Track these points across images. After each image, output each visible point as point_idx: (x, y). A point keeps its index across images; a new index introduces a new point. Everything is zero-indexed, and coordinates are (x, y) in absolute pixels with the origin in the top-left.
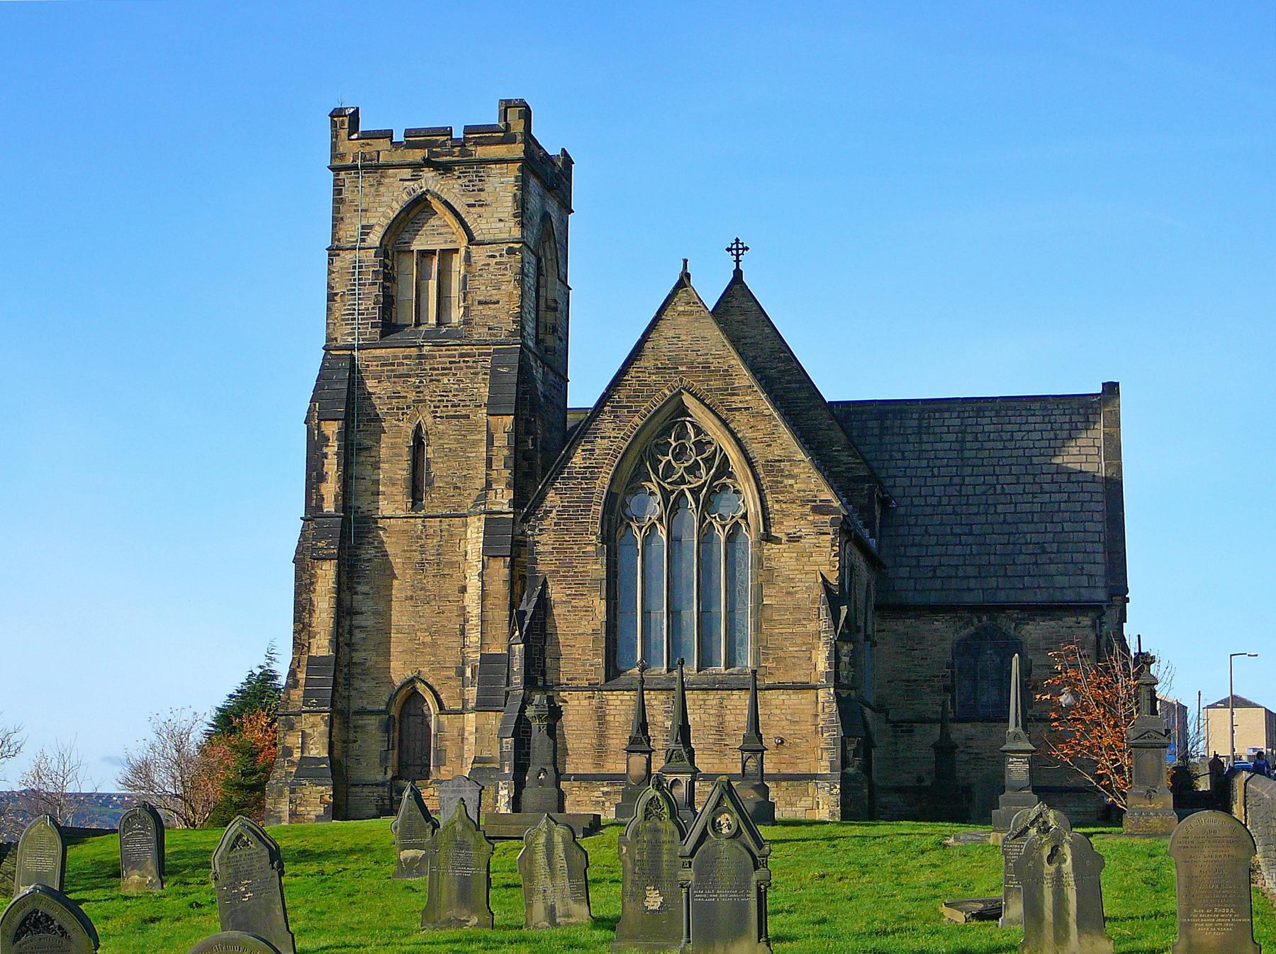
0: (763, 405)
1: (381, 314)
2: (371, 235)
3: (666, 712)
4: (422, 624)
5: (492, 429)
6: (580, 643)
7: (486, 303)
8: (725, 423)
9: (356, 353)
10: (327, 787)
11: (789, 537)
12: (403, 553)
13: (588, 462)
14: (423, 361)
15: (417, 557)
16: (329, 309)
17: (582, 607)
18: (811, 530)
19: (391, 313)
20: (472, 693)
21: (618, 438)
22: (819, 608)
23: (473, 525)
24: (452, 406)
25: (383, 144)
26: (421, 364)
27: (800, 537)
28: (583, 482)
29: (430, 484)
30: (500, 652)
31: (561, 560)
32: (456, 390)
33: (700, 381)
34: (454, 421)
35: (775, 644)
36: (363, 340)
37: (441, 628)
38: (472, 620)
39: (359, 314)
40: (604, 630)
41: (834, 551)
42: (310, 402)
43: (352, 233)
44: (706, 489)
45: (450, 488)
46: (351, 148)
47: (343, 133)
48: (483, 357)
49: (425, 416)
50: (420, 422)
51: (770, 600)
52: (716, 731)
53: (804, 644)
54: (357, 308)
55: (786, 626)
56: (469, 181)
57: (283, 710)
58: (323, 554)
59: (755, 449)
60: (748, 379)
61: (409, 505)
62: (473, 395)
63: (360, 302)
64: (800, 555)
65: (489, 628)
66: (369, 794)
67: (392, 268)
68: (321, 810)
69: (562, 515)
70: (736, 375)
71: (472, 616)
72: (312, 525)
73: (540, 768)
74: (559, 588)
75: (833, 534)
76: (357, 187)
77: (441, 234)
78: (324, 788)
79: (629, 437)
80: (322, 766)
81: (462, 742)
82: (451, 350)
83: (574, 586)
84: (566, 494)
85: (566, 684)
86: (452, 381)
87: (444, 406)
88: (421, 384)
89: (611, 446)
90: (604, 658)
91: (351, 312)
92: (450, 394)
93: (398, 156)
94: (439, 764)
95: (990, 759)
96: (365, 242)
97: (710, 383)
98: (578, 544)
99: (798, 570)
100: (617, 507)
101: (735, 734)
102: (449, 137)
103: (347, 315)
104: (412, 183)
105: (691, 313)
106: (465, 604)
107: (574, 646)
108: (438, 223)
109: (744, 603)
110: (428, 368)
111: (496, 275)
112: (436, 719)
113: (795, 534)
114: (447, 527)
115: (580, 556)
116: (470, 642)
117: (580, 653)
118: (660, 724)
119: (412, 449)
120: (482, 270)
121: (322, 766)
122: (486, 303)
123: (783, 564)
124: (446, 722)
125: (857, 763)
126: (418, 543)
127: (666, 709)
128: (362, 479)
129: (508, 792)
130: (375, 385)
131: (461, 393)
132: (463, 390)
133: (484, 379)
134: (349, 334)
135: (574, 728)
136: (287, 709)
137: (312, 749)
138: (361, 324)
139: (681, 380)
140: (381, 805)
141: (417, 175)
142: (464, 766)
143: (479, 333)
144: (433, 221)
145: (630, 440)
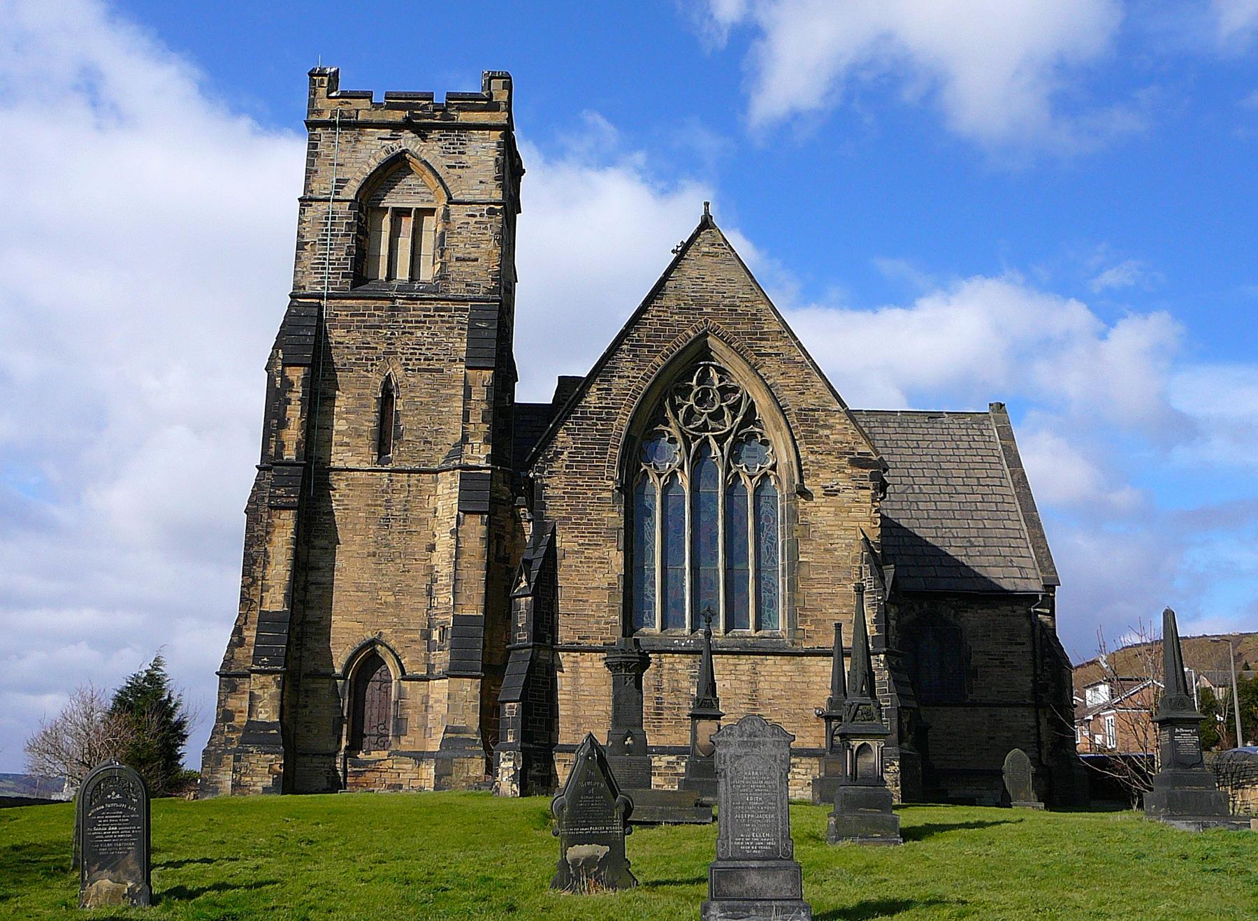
0: (794, 352)
1: (353, 265)
2: (345, 188)
3: (692, 677)
4: (385, 582)
5: (470, 382)
6: (593, 598)
7: (464, 260)
8: (754, 368)
9: (324, 303)
10: (277, 755)
11: (826, 491)
12: (366, 508)
13: (604, 402)
14: (396, 313)
15: (382, 512)
16: (298, 257)
17: (597, 559)
18: (850, 484)
19: (362, 268)
20: (442, 659)
21: (638, 378)
22: (861, 568)
23: (444, 481)
24: (425, 360)
25: (363, 104)
26: (393, 315)
27: (838, 491)
28: (599, 422)
29: (399, 437)
30: (475, 614)
31: (573, 505)
32: (430, 343)
33: (728, 323)
34: (427, 375)
35: (813, 605)
36: (333, 289)
37: (406, 588)
38: (442, 580)
39: (330, 264)
40: (621, 584)
41: (875, 506)
42: (273, 349)
43: (326, 186)
44: (732, 436)
45: (420, 442)
46: (328, 108)
47: (322, 92)
48: (460, 312)
49: (396, 368)
50: (389, 374)
51: (807, 557)
52: (749, 699)
53: (845, 605)
54: (328, 258)
55: (823, 586)
56: (450, 144)
57: (226, 670)
58: (282, 502)
59: (788, 397)
60: (778, 324)
61: (375, 458)
62: (448, 349)
63: (331, 252)
64: (839, 510)
65: (463, 588)
66: (320, 765)
67: (366, 223)
68: (269, 782)
69: (575, 457)
70: (765, 320)
71: (442, 576)
72: (268, 475)
73: (627, 731)
74: (570, 537)
75: (874, 489)
76: (333, 142)
77: (418, 193)
78: (274, 756)
79: (650, 377)
80: (271, 732)
81: (426, 711)
82: (426, 304)
83: (588, 535)
84: (580, 435)
85: (577, 644)
86: (425, 335)
87: (416, 359)
88: (392, 336)
89: (630, 385)
90: (621, 615)
91: (322, 261)
92: (424, 348)
93: (377, 116)
94: (399, 734)
95: (934, 742)
96: (339, 195)
97: (737, 326)
98: (592, 489)
99: (836, 526)
100: (635, 452)
101: (770, 704)
102: (431, 102)
103: (317, 264)
104: (390, 142)
105: (716, 255)
106: (433, 563)
107: (587, 601)
108: (414, 183)
109: (773, 561)
110: (401, 320)
111: (475, 234)
112: (398, 685)
113: (832, 487)
114: (416, 482)
115: (595, 503)
116: (438, 603)
117: (594, 609)
118: (685, 690)
119: (380, 400)
120: (461, 228)
121: (271, 732)
122: (464, 260)
123: (819, 519)
124: (408, 689)
125: (910, 736)
126: (383, 497)
127: (692, 674)
128: (325, 428)
129: (514, 764)
130: (343, 334)
131: (435, 347)
132: (437, 344)
133: (459, 334)
134: (318, 283)
135: (586, 693)
136: (230, 668)
137: (261, 712)
138: (331, 274)
139: (706, 321)
140: (332, 777)
141: (396, 135)
142: (427, 736)
143: (456, 289)
144: (409, 180)
145: (651, 381)
